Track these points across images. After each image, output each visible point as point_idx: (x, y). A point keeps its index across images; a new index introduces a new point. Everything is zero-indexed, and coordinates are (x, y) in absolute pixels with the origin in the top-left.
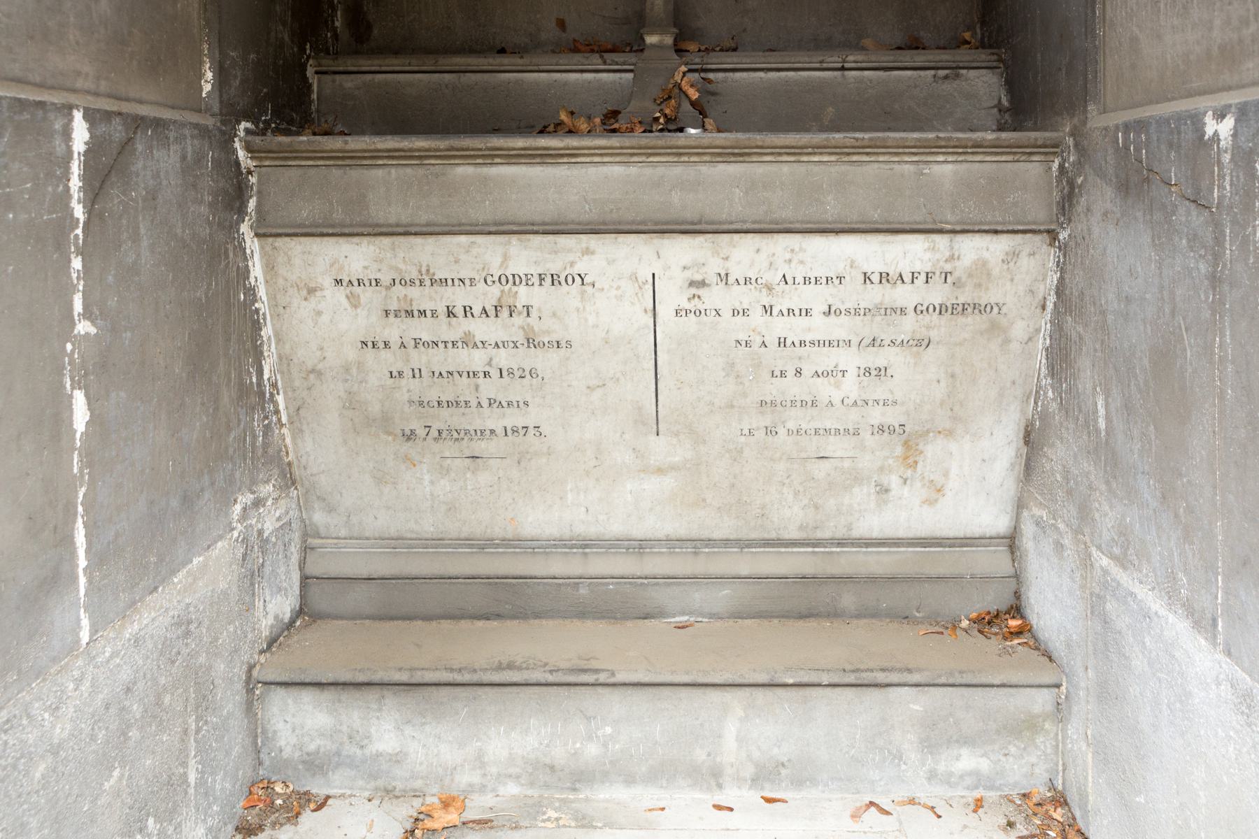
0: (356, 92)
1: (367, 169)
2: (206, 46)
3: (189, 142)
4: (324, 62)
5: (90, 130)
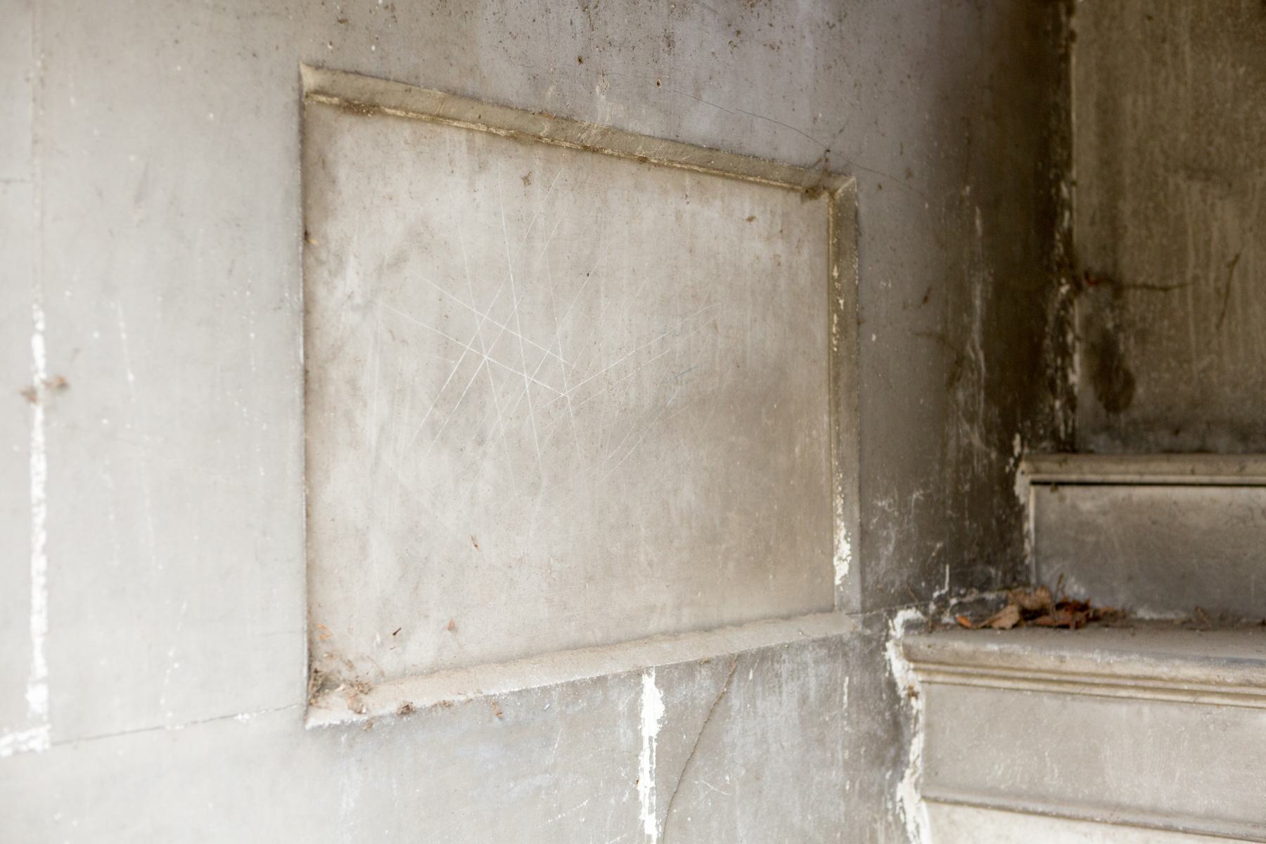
0: (1101, 520)
1: (1101, 702)
2: (839, 501)
3: (811, 671)
4: (1045, 466)
5: (666, 703)
